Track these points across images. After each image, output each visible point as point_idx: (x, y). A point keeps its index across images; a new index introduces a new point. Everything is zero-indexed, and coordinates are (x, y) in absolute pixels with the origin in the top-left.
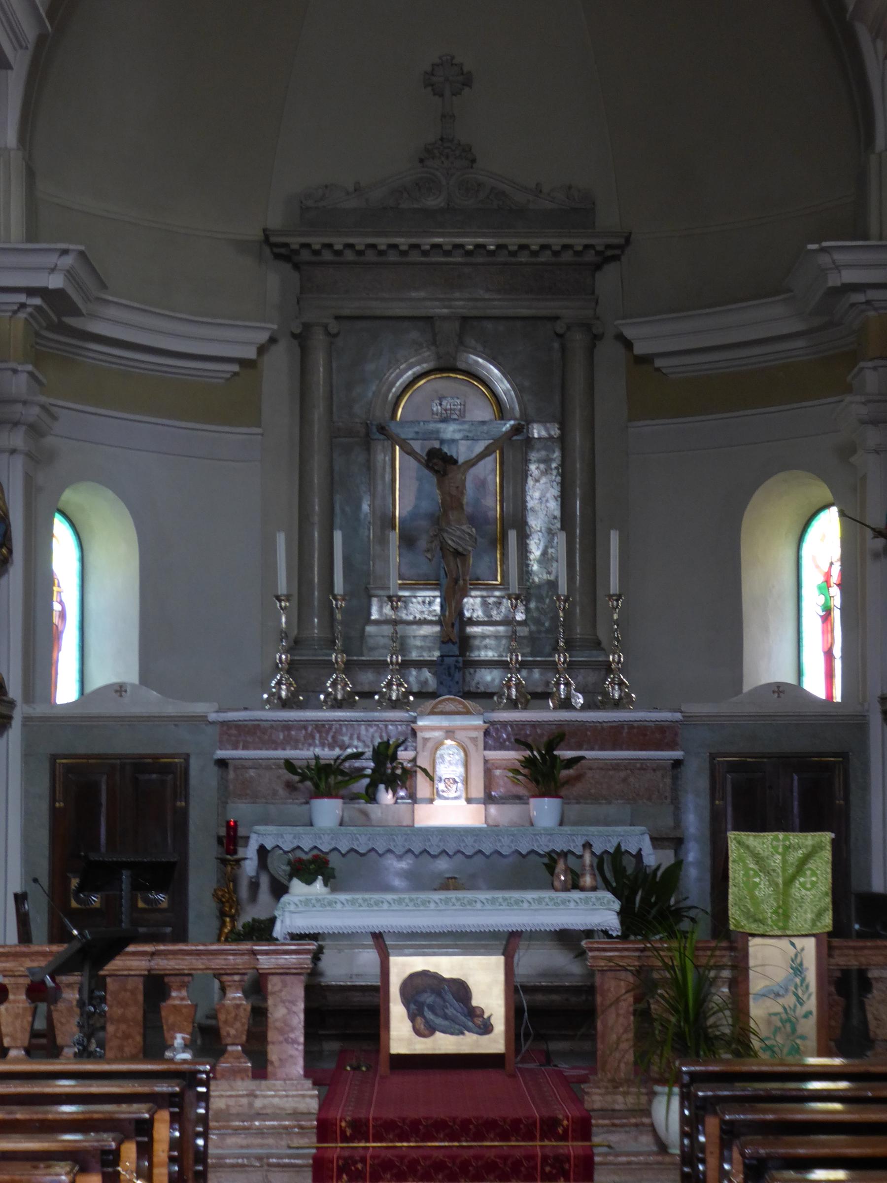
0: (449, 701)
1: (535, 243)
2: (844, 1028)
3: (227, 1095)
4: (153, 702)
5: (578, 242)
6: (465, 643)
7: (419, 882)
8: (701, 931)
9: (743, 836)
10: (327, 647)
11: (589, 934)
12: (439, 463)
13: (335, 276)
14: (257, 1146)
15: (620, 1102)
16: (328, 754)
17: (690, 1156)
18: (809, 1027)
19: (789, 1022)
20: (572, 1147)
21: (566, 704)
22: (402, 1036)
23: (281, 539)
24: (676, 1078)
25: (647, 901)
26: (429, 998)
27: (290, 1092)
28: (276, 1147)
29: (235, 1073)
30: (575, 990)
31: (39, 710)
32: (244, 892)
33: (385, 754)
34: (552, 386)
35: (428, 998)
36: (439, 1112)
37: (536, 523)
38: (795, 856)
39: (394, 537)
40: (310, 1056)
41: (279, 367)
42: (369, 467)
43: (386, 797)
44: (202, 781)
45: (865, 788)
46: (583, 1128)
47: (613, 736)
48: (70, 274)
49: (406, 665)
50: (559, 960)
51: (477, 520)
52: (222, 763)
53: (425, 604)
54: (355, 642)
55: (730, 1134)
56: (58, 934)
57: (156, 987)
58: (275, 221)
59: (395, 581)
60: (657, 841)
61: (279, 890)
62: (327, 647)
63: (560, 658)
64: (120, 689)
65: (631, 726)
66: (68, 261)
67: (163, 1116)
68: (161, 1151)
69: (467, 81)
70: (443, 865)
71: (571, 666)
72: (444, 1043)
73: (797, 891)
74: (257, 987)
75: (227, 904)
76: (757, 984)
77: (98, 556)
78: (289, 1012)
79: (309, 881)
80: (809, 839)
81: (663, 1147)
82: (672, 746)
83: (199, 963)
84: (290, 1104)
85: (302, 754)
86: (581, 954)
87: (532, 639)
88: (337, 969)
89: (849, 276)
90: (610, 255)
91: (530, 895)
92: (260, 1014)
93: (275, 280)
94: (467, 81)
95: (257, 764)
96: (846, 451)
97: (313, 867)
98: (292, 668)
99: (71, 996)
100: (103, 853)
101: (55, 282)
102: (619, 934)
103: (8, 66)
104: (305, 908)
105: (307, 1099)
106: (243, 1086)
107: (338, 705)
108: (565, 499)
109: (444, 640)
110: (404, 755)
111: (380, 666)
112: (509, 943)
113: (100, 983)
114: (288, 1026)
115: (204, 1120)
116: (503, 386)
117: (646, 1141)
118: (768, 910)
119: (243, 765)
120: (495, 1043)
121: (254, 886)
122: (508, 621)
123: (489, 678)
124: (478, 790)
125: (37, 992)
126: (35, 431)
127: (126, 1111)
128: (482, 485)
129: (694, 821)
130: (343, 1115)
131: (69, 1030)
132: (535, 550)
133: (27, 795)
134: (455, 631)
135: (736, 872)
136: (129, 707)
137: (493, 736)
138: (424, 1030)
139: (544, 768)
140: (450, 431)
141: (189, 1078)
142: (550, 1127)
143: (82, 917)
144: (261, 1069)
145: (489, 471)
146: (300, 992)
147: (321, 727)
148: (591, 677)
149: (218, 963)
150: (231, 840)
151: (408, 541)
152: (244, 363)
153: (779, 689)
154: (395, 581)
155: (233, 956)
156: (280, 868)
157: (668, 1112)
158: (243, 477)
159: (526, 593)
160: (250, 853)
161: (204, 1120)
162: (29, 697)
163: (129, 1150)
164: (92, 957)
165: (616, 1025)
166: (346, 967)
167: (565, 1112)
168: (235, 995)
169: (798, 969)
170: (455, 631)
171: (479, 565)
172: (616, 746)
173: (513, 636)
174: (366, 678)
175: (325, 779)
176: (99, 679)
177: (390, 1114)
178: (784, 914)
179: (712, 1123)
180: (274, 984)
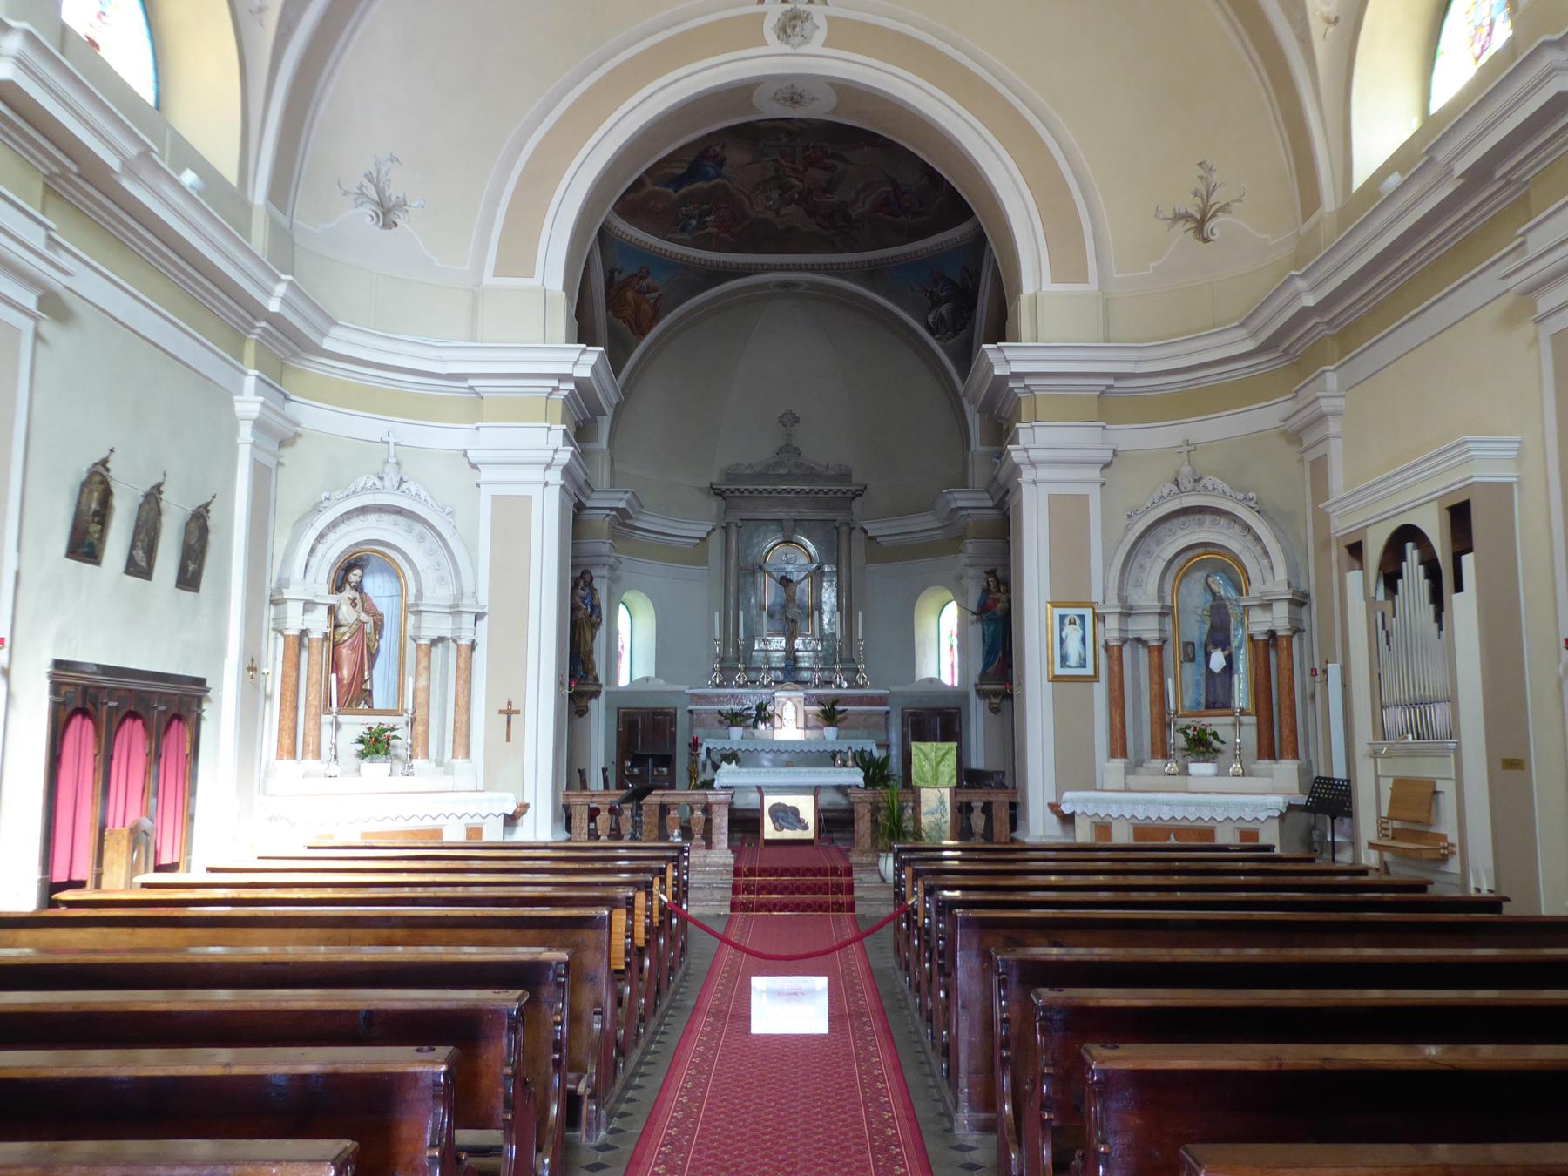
0: (789, 685)
1: (826, 489)
2: (962, 829)
3: (696, 856)
4: (661, 685)
5: (844, 489)
6: (796, 660)
7: (776, 764)
8: (897, 785)
9: (922, 745)
10: (735, 660)
11: (849, 787)
12: (785, 582)
13: (739, 501)
14: (708, 879)
15: (865, 860)
16: (737, 708)
17: (898, 884)
18: (947, 827)
19: (938, 826)
20: (844, 880)
21: (840, 686)
22: (769, 831)
23: (717, 615)
24: (891, 849)
25: (875, 772)
26: (781, 814)
27: (721, 855)
28: (716, 879)
29: (698, 847)
30: (844, 811)
31: (612, 688)
32: (700, 767)
33: (761, 708)
34: (833, 549)
35: (781, 814)
36: (786, 865)
37: (826, 608)
38: (941, 753)
39: (765, 614)
40: (730, 840)
41: (716, 541)
42: (754, 583)
43: (761, 726)
44: (682, 720)
45: (968, 723)
46: (849, 872)
47: (859, 700)
48: (628, 502)
49: (770, 669)
50: (838, 800)
51: (801, 607)
52: (691, 712)
53: (779, 643)
54: (748, 659)
55: (917, 875)
56: (621, 786)
57: (664, 809)
58: (715, 479)
59: (765, 632)
60: (879, 746)
61: (716, 767)
62: (735, 660)
63: (837, 667)
64: (647, 679)
65: (867, 696)
66: (627, 496)
67: (671, 866)
68: (669, 881)
69: (797, 420)
70: (785, 757)
71: (842, 670)
72: (788, 834)
73: (941, 768)
74: (707, 809)
75: (693, 774)
76: (924, 809)
77: (638, 623)
78: (721, 821)
79: (730, 763)
80: (947, 745)
81: (884, 880)
82: (884, 704)
83: (682, 799)
84: (721, 861)
85: (726, 708)
86: (847, 795)
87: (824, 658)
88: (742, 802)
89: (960, 504)
90: (859, 493)
91: (825, 770)
92: (708, 821)
93: (715, 504)
94: (797, 420)
95: (705, 712)
96: (959, 578)
97: (731, 757)
98: (721, 670)
99: (628, 813)
100: (639, 751)
101: (622, 505)
102: (1039, 828)
103: (604, 414)
104: (728, 775)
105: (728, 858)
106: (702, 852)
107: (741, 686)
108: (839, 597)
109: (787, 659)
110: (769, 708)
111: (759, 670)
112: (816, 790)
113: (640, 807)
114: (720, 827)
115: (687, 868)
116: (812, 549)
117: (876, 877)
118: (929, 777)
119: (700, 713)
120: (810, 834)
121: (704, 765)
122: (814, 650)
123: (805, 675)
124: (801, 724)
125: (612, 811)
126: (612, 568)
127: (654, 864)
128: (803, 591)
129: (895, 738)
130: (745, 866)
131: (627, 828)
132: (826, 620)
133: (607, 726)
134: (791, 656)
135: (915, 760)
136: (650, 687)
137: (808, 700)
138: (780, 828)
139: (830, 715)
140: (790, 568)
141: (681, 849)
142: (834, 871)
143: (632, 778)
144: (709, 845)
145: (806, 586)
146: (726, 812)
147: (733, 696)
148: (850, 675)
149: (690, 799)
150: (695, 745)
151: (771, 615)
152: (701, 539)
153: (931, 680)
154: (765, 632)
155: (697, 796)
156: (716, 758)
157: (888, 865)
158: (700, 589)
159: (822, 638)
160: (703, 751)
161: (687, 868)
162: (608, 683)
163: (657, 881)
164: (637, 796)
165: (863, 826)
166: (747, 801)
167: (841, 865)
168: (698, 813)
169: (942, 803)
170: (791, 656)
171: (801, 625)
172: (861, 704)
173: (816, 657)
174: (753, 675)
175: (735, 719)
176: (638, 675)
177: (765, 865)
178: (936, 778)
179: (908, 870)
180: (715, 808)
